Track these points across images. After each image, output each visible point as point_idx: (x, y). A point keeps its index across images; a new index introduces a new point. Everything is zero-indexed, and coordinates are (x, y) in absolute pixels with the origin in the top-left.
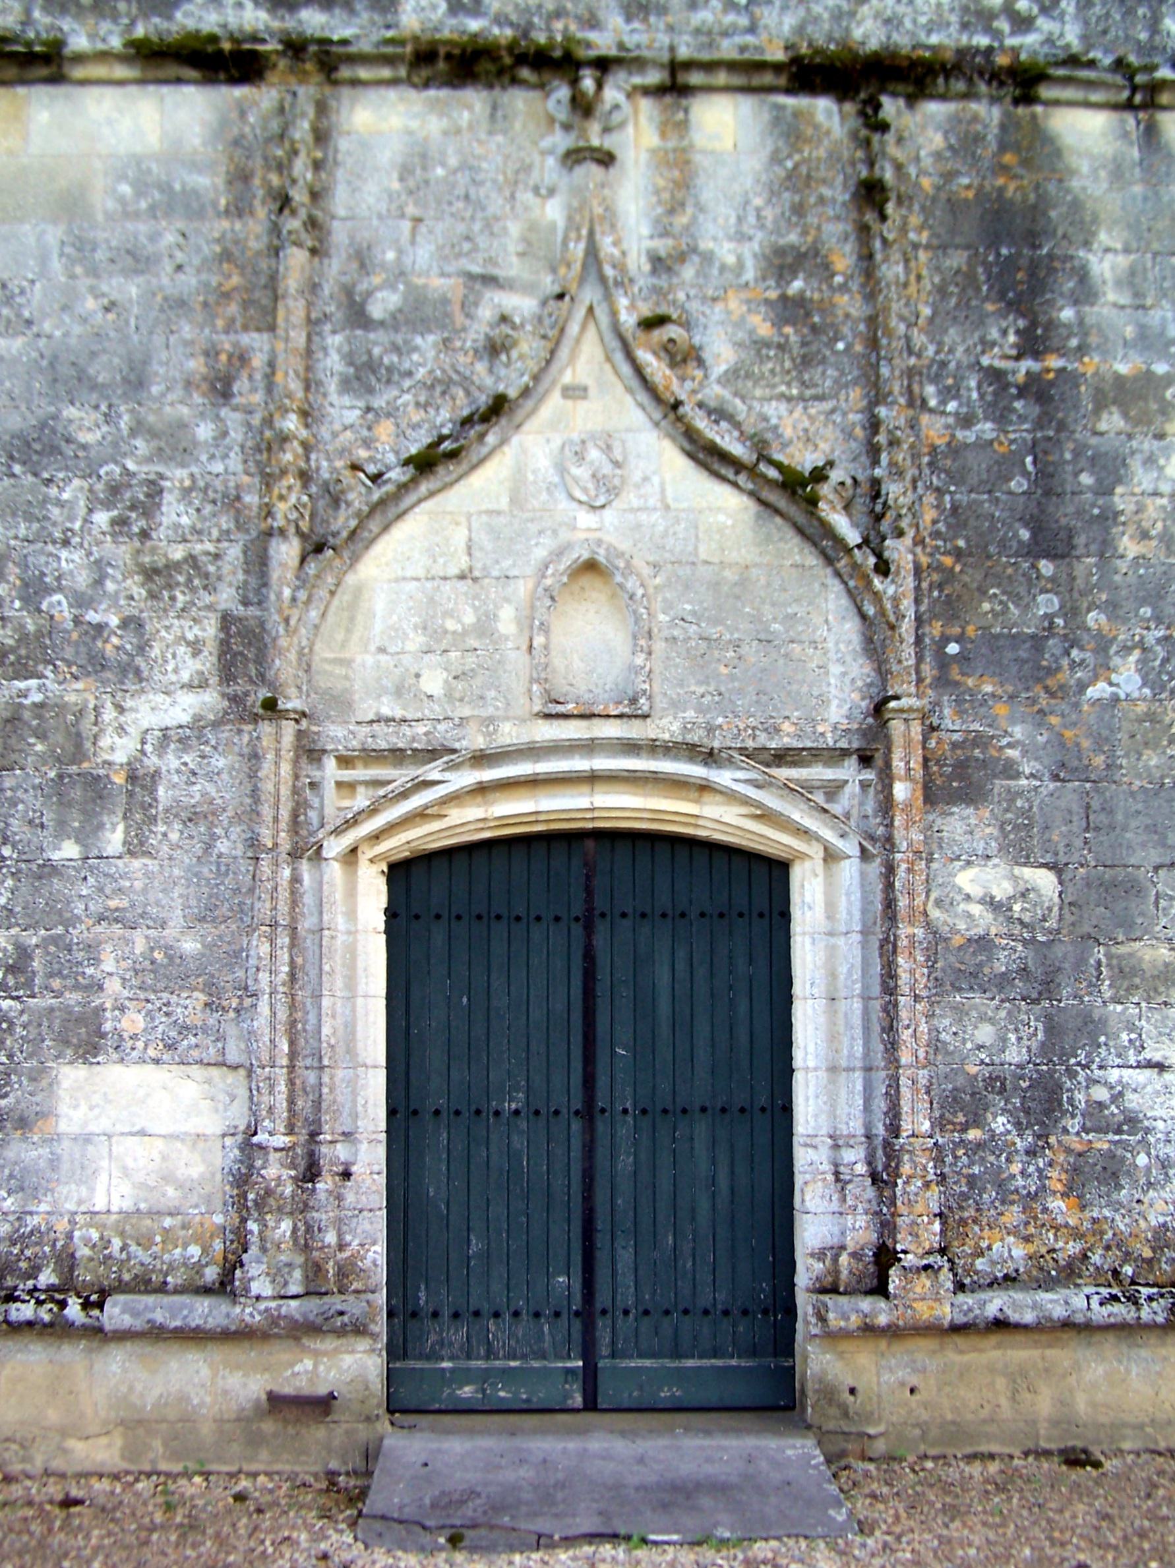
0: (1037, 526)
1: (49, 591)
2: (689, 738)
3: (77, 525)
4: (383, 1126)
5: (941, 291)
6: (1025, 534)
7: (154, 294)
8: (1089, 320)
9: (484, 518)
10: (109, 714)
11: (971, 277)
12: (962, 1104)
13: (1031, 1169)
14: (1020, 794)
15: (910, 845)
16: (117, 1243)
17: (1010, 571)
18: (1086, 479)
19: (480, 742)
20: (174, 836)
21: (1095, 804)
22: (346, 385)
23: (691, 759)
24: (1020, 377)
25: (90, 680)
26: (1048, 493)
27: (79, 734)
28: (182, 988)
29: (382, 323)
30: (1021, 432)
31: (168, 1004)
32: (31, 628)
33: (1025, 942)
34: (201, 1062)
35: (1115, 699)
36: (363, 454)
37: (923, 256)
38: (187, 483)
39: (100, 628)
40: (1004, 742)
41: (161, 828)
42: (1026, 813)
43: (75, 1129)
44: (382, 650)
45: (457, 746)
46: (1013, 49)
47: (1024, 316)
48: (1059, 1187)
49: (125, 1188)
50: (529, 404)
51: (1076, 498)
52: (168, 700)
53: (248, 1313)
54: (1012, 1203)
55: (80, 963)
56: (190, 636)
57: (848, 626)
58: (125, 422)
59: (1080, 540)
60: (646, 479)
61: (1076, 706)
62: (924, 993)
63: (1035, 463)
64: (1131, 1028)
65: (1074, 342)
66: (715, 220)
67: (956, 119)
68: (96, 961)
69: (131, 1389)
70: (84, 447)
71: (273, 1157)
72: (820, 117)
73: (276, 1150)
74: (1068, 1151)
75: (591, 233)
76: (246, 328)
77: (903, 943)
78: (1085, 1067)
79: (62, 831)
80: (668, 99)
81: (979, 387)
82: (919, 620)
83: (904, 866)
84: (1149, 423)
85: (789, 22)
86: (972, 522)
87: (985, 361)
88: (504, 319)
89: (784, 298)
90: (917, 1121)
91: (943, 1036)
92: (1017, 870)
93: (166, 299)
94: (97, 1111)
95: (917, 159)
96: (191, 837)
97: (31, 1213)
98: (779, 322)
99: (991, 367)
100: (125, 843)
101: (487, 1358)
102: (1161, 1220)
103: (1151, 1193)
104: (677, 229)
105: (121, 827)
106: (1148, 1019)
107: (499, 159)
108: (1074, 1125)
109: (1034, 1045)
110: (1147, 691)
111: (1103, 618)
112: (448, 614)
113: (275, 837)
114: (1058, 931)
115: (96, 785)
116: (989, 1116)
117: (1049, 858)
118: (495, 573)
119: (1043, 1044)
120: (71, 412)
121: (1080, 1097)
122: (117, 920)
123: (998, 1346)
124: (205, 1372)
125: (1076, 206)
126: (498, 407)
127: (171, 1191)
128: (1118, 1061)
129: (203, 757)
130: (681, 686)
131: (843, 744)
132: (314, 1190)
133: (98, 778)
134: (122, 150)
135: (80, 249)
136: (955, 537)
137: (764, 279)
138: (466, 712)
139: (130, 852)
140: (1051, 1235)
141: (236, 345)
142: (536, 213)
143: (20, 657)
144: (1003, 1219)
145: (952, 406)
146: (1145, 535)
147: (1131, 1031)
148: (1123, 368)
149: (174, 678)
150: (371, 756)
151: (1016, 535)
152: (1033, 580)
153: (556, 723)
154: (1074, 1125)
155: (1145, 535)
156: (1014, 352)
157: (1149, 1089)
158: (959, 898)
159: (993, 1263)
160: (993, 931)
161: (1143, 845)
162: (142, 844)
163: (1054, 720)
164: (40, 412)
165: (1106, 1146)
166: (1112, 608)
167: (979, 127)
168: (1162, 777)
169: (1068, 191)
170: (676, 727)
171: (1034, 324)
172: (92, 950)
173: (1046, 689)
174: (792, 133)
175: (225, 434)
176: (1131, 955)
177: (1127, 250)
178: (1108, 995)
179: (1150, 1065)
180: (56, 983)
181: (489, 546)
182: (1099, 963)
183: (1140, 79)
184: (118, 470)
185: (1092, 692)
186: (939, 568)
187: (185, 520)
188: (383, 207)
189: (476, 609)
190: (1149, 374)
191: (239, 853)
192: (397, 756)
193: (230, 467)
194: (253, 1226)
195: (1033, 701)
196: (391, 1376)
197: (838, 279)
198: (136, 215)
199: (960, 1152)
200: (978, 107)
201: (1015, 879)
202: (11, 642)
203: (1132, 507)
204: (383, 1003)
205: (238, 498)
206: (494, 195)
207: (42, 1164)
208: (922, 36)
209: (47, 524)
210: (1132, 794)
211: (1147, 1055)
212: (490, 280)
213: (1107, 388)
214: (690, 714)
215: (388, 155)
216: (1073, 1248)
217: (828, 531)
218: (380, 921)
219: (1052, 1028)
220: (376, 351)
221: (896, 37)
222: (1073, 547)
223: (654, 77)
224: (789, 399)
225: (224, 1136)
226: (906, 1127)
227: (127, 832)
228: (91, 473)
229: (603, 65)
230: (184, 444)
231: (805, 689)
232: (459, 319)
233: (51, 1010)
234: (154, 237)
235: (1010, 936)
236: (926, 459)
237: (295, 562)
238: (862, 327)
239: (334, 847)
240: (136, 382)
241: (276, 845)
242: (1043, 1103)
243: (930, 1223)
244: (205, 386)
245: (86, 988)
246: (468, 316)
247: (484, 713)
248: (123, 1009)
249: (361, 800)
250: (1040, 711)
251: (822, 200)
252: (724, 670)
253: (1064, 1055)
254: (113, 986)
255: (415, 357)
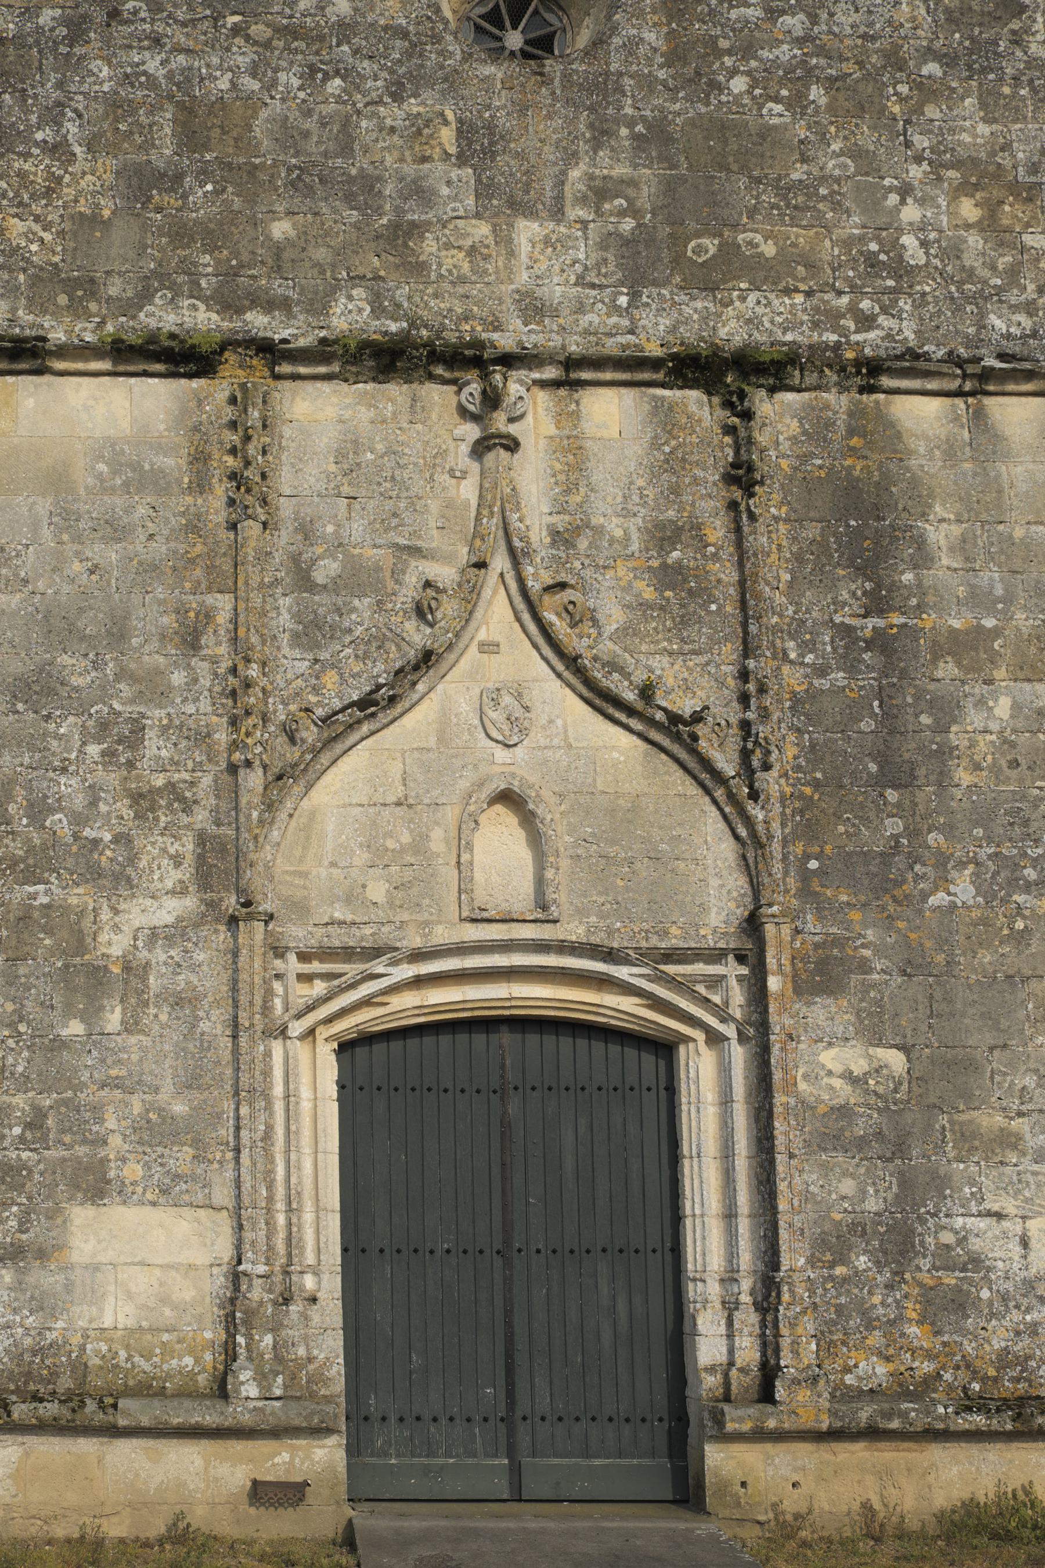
0: (883, 759)
1: (52, 811)
2: (593, 940)
3: (73, 756)
4: (339, 1261)
5: (799, 558)
6: (873, 767)
7: (131, 560)
8: (926, 583)
9: (416, 755)
10: (105, 915)
11: (824, 545)
12: (833, 1246)
13: (890, 1300)
14: (874, 986)
15: (783, 1028)
16: (123, 1354)
17: (860, 799)
18: (925, 719)
19: (417, 942)
20: (164, 1017)
21: (938, 994)
22: (296, 639)
23: (593, 958)
24: (868, 633)
25: (89, 886)
26: (892, 732)
27: (81, 931)
28: (173, 1143)
29: (325, 587)
30: (868, 680)
31: (162, 1156)
32: (37, 841)
33: (879, 1110)
34: (191, 1205)
35: (953, 906)
36: (313, 699)
37: (783, 528)
38: (165, 722)
39: (96, 842)
40: (859, 943)
41: (152, 1011)
42: (879, 1003)
43: (85, 1260)
44: (333, 864)
45: (398, 944)
46: (857, 343)
47: (870, 580)
48: (914, 1315)
49: (130, 1309)
50: (452, 657)
51: (917, 736)
52: (156, 904)
53: (238, 1413)
54: (874, 1329)
55: (86, 1122)
56: (172, 851)
57: (724, 846)
58: (110, 668)
59: (921, 772)
60: (551, 722)
61: (920, 912)
62: (797, 1152)
63: (880, 706)
64: (972, 1182)
65: (914, 601)
66: (604, 498)
67: (809, 407)
68: (101, 1121)
69: (137, 1475)
70: (77, 689)
71: (257, 1282)
72: (693, 408)
73: (258, 1276)
74: (920, 1284)
75: (503, 511)
76: (209, 590)
77: (778, 1110)
78: (934, 1215)
79: (69, 1011)
80: (562, 392)
81: (832, 642)
82: (785, 842)
83: (778, 1046)
84: (981, 670)
85: (665, 322)
86: (828, 758)
87: (838, 619)
88: (428, 584)
89: (664, 566)
90: (794, 1258)
91: (812, 1188)
92: (871, 1051)
93: (140, 563)
94: (104, 1244)
95: (777, 443)
96: (178, 1018)
97: (49, 1329)
98: (659, 590)
99: (843, 623)
100: (122, 1023)
101: (427, 1456)
102: (1003, 1344)
103: (994, 1322)
104: (571, 508)
105: (118, 1009)
106: (987, 1176)
107: (419, 445)
108: (925, 1263)
109: (890, 1196)
110: (980, 899)
111: (941, 838)
112: (389, 835)
113: (251, 1018)
114: (908, 1102)
115: (98, 974)
116: (853, 1255)
117: (898, 1040)
118: (427, 801)
119: (897, 1195)
120: (65, 659)
121: (930, 1240)
122: (117, 1087)
123: (866, 1449)
124: (199, 1462)
125: (914, 482)
126: (427, 659)
127: (168, 1312)
128: (962, 1211)
129: (187, 952)
130: (586, 897)
131: (722, 945)
132: (287, 1312)
133: (97, 968)
134: (98, 434)
135: (66, 518)
136: (814, 771)
137: (647, 550)
138: (406, 916)
139: (126, 1030)
140: (908, 1355)
141: (202, 604)
142: (453, 492)
143: (28, 866)
144: (868, 1342)
145: (809, 658)
146: (977, 767)
147: (972, 1185)
148: (956, 624)
149: (160, 886)
150: (326, 954)
151: (865, 768)
152: (882, 808)
153: (481, 926)
154: (925, 1263)
155: (977, 767)
156: (862, 611)
157: (989, 1234)
158: (822, 1073)
159: (860, 1379)
160: (852, 1101)
161: (980, 1029)
162: (137, 1023)
163: (901, 924)
164: (37, 658)
165: (953, 1282)
166: (949, 830)
167: (830, 414)
168: (995, 972)
169: (908, 469)
170: (581, 930)
171: (879, 586)
172: (97, 1111)
173: (894, 897)
174: (666, 420)
175: (196, 680)
176: (971, 1122)
177: (959, 521)
178: (951, 1155)
179: (989, 1214)
180: (67, 1139)
181: (421, 778)
182: (943, 1128)
183: (970, 369)
184: (106, 709)
185: (932, 900)
186: (802, 797)
187: (164, 753)
188: (321, 486)
189: (411, 831)
190: (979, 629)
191: (219, 1032)
192: (348, 954)
193: (203, 709)
194: (240, 1339)
195: (883, 908)
196: (350, 1467)
197: (711, 549)
198: (113, 490)
199: (829, 1286)
200: (830, 397)
201: (870, 1057)
202: (21, 853)
203: (966, 743)
204: (337, 1157)
205: (209, 735)
206: (416, 477)
207: (59, 1288)
208: (779, 336)
209: (46, 754)
210: (969, 986)
211: (987, 1206)
212: (415, 551)
213: (943, 640)
214: (593, 919)
215: (326, 440)
216: (927, 1367)
217: (706, 764)
218: (333, 1090)
219: (905, 1183)
220: (321, 611)
221: (756, 335)
222: (915, 778)
223: (551, 373)
224: (671, 654)
225: (211, 1266)
226: (785, 1263)
227: (124, 1013)
228: (83, 711)
229: (508, 361)
230: (162, 688)
231: (689, 898)
232: (390, 585)
233: (64, 1160)
234: (129, 510)
235: (868, 1106)
236: (788, 704)
237: (261, 789)
238: (732, 591)
239: (296, 1028)
240: (118, 634)
241: (252, 1025)
242: (898, 1244)
243: (808, 1343)
244: (177, 639)
245: (93, 1142)
246: (397, 582)
247: (420, 918)
248: (124, 1160)
249: (319, 988)
250: (889, 917)
251: (696, 481)
252: (620, 883)
253: (915, 1206)
254: (115, 1141)
255: (353, 617)
